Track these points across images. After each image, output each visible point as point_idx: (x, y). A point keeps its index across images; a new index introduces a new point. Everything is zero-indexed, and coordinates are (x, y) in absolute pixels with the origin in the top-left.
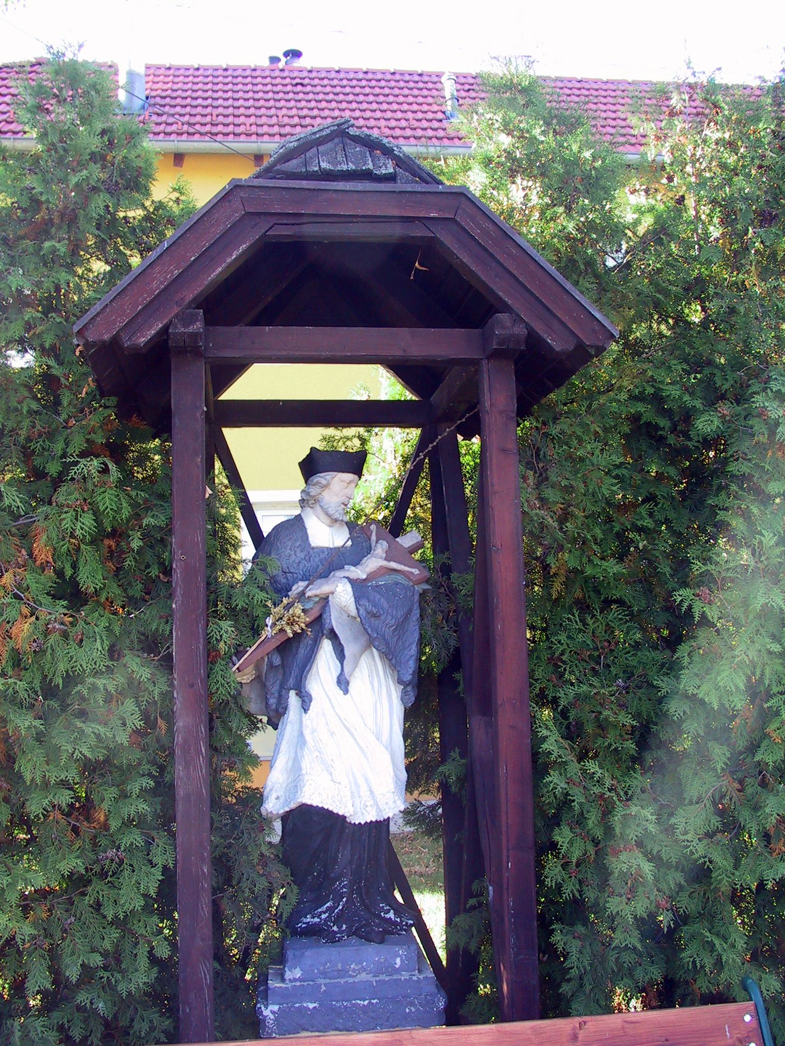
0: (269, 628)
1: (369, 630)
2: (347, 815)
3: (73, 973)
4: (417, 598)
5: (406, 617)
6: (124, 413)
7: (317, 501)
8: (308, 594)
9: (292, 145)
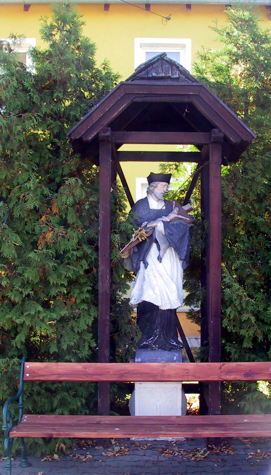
0: (133, 238)
1: (169, 240)
2: (159, 306)
3: (65, 347)
4: (188, 229)
5: (184, 236)
6: (82, 158)
7: (152, 192)
8: (148, 226)
9: (142, 66)
